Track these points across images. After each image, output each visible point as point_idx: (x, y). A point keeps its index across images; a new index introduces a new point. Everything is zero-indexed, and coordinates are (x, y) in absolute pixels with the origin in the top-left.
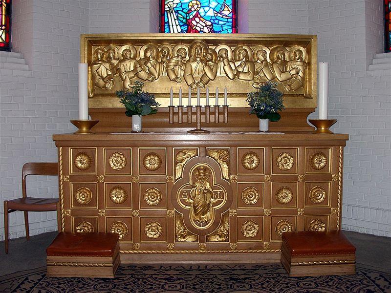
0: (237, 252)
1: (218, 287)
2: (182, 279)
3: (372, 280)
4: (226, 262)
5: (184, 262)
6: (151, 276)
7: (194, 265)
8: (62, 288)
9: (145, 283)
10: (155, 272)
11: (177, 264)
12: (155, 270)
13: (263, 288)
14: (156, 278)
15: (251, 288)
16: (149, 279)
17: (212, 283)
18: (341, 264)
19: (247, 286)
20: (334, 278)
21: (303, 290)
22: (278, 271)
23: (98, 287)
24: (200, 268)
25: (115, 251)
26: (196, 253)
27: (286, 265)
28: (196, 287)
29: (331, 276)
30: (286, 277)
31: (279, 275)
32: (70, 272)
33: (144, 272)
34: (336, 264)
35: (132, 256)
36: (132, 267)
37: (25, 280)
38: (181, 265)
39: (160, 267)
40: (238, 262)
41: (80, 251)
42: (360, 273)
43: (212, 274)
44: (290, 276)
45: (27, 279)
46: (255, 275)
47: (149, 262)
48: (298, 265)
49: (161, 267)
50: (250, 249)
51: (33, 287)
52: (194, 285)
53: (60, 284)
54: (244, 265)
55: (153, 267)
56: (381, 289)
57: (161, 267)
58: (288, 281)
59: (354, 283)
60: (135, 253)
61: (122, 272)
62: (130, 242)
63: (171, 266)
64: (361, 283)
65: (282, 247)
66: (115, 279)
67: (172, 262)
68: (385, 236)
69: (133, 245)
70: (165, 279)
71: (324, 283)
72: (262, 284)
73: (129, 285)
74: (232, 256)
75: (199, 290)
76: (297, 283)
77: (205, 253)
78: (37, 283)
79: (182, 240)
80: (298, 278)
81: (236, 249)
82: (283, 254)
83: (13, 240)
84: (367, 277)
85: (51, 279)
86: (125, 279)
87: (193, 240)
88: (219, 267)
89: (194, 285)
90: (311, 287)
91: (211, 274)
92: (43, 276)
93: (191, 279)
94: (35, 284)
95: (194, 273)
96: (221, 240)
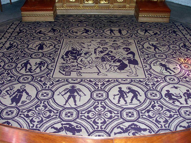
0: (113, 9)
1: (103, 25)
2: (87, 21)
3: (176, 26)
4: (108, 14)
5: (88, 13)
6: (72, 20)
7: (93, 15)
8: (30, 27)
9: (69, 23)
10: (74, 18)
11: (84, 14)
12: (74, 17)
13: (125, 26)
14: (74, 21)
15: (119, 26)
16: (71, 21)
17: (101, 23)
18: (163, 17)
19: (117, 26)
20: (159, 24)
21: (144, 29)
22: (132, 19)
23: (47, 26)
24: (95, 16)
25: (54, 8)
26: (93, 9)
27: (137, 16)
28: (93, 25)
29: (157, 23)
30: (136, 22)
31: (133, 21)
32: (33, 19)
33: (69, 18)
34: (160, 17)
35: (62, 11)
36: (63, 16)
37: (13, 24)
38: (86, 15)
39: (76, 16)
40: (113, 14)
41: (37, 9)
42: (171, 22)
43: (101, 19)
44: (138, 22)
45: (13, 23)
46: (121, 20)
47: (71, 13)
48: (142, 17)
49: (77, 15)
50: (120, 8)
51: (16, 27)
52: (92, 24)
53: (29, 25)
54: (116, 15)
55: (73, 16)
56: (180, 30)
57: (77, 15)
58: (137, 24)
59: (168, 27)
60: (64, 9)
61: (58, 18)
62: (61, 4)
63: (81, 15)
64: (171, 27)
65: (136, 7)
66: (55, 22)
67: (82, 13)
68: (186, 5)
69: (63, 5)
70: (79, 21)
71: (154, 26)
72: (124, 25)
73: (61, 24)
74: (111, 11)
75: (95, 27)
76: (141, 25)
77: (98, 9)
78: (18, 25)
79: (87, 2)
80: (142, 23)
81: (113, 8)
82: (136, 11)
83: (4, 4)
84: (175, 24)
85: (24, 23)
86: (60, 22)
87: (92, 3)
88: (105, 16)
89: (92, 24)
90: (148, 27)
91: (100, 19)
92: (21, 22)
93: (91, 21)
94: (17, 26)
95: (93, 19)
96: (106, 3)
